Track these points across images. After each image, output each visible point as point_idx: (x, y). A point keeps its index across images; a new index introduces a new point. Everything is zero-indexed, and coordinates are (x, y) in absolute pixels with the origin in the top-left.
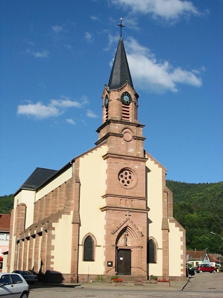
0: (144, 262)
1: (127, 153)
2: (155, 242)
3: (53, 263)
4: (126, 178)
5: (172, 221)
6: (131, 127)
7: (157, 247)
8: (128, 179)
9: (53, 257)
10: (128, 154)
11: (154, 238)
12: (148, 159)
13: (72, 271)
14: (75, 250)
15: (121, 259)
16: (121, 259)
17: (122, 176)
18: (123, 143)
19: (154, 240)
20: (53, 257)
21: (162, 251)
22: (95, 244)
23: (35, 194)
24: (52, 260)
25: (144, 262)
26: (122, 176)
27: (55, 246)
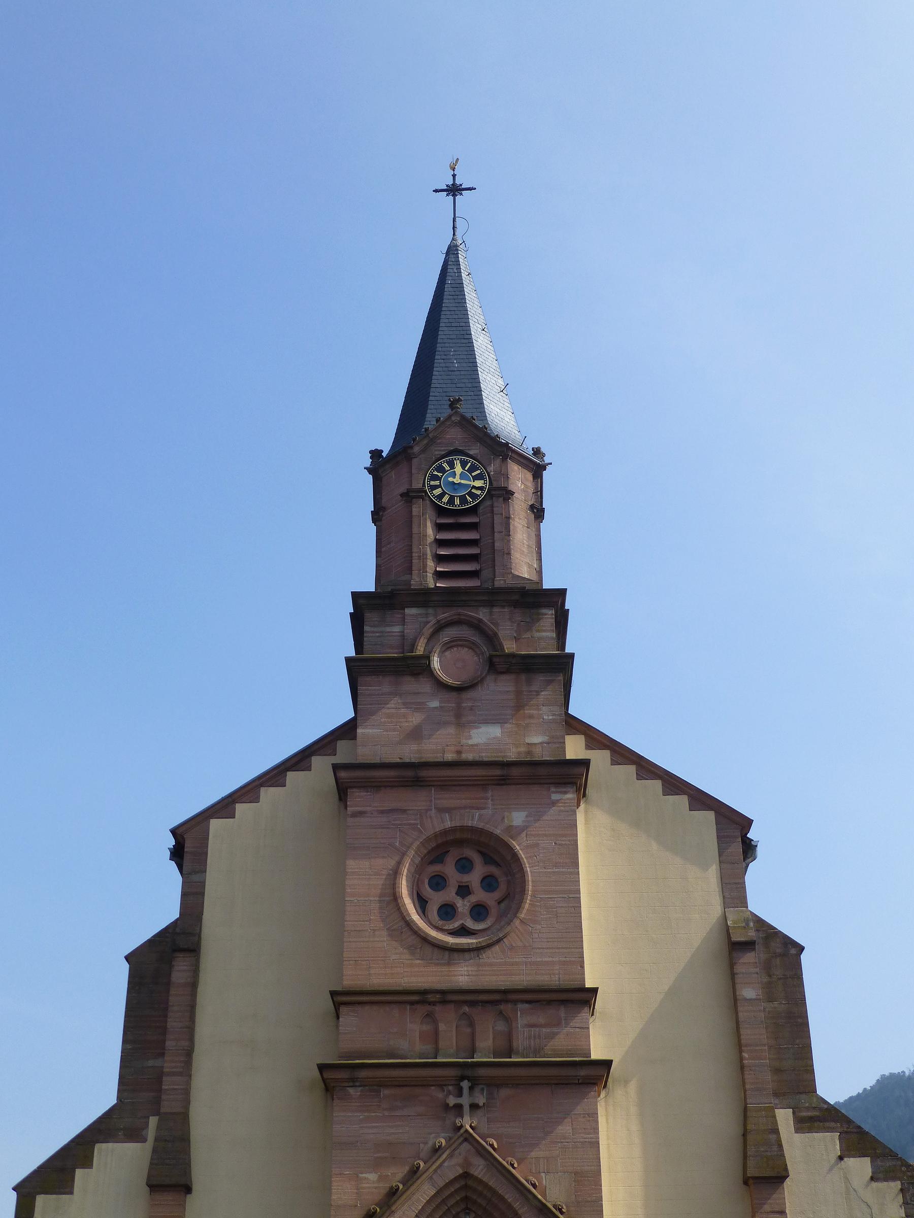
5: (811, 1119)
17: (464, 866)
18: (435, 704)
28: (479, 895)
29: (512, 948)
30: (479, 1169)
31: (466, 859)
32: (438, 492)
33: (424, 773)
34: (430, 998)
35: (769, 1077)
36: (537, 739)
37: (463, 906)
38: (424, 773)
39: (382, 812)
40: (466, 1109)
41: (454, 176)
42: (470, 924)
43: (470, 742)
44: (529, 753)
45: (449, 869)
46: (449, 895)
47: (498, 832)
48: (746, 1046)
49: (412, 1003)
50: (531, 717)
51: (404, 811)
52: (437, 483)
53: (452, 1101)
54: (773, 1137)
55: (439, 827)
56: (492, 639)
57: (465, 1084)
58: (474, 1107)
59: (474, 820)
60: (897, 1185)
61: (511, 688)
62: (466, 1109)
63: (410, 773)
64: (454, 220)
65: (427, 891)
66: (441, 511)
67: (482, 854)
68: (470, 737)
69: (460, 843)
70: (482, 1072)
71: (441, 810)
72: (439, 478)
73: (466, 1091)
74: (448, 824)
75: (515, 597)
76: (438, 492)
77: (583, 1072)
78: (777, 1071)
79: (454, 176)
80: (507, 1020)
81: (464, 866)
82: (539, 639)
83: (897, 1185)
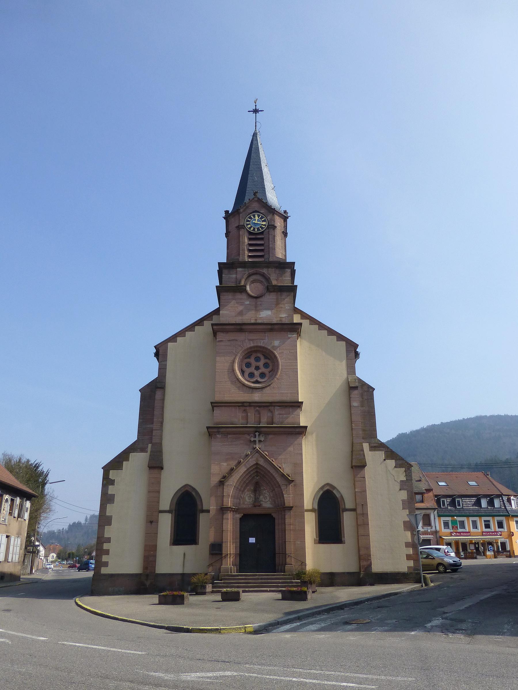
0: (299, 543)
1: (256, 320)
2: (337, 496)
3: (107, 552)
4: (257, 368)
5: (375, 447)
6: (265, 271)
7: (342, 507)
8: (263, 370)
9: (108, 540)
10: (259, 321)
11: (334, 488)
12: (300, 324)
13: (145, 568)
14: (151, 522)
15: (252, 540)
16: (252, 540)
17: (257, 359)
18: (248, 303)
19: (334, 492)
20: (108, 540)
21: (306, 508)
22: (199, 507)
23: (162, 370)
24: (106, 546)
25: (299, 543)
26: (248, 365)
27: (193, 546)
28: (263, 370)
30: (261, 462)
32: (249, 226)
33: (244, 327)
35: (361, 433)
36: (283, 315)
39: (229, 340)
40: (257, 442)
42: (259, 380)
43: (260, 316)
45: (252, 360)
47: (269, 348)
56: (268, 280)
58: (260, 441)
59: (261, 344)
60: (404, 469)
62: (257, 442)
63: (238, 327)
65: (244, 368)
66: (250, 233)
69: (256, 352)
71: (250, 340)
74: (252, 345)
76: (249, 226)
78: (364, 430)
81: (257, 359)
83: (404, 469)
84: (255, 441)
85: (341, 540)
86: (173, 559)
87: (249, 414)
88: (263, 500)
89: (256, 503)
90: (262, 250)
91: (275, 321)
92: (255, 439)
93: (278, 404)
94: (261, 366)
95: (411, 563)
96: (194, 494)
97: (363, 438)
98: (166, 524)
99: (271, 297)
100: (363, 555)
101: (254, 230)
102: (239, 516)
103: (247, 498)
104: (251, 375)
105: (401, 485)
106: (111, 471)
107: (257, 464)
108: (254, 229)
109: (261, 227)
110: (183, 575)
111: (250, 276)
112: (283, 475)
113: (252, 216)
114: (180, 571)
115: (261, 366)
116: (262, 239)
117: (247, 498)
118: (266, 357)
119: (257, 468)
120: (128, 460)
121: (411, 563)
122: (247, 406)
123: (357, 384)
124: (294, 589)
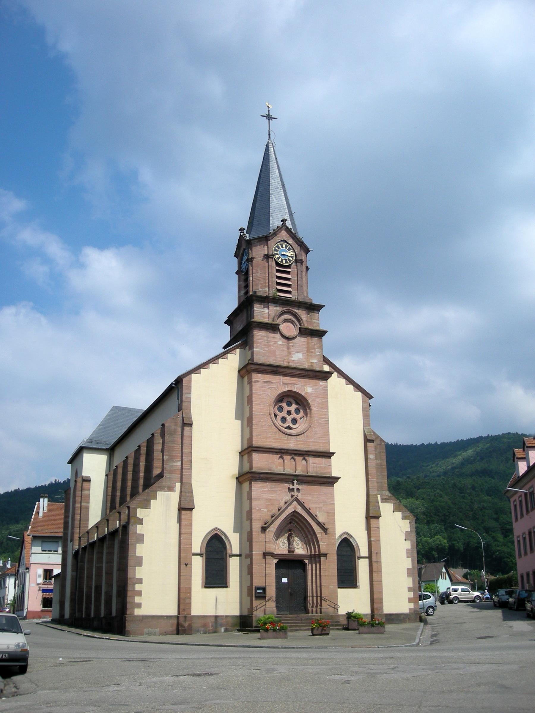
1: (289, 362)
2: (354, 544)
4: (289, 413)
5: (386, 499)
8: (294, 415)
11: (351, 536)
14: (184, 564)
17: (289, 404)
18: (280, 343)
22: (229, 551)
27: (225, 589)
28: (294, 415)
29: (307, 436)
30: (299, 510)
31: (290, 402)
32: (277, 256)
33: (279, 369)
34: (283, 451)
35: (376, 485)
36: (314, 361)
37: (289, 418)
38: (279, 369)
39: (265, 382)
40: (295, 490)
41: (269, 111)
42: (292, 426)
43: (293, 359)
44: (312, 366)
45: (284, 405)
46: (284, 414)
47: (303, 394)
48: (185, 469)
49: (276, 452)
50: (312, 352)
51: (272, 382)
52: (277, 252)
53: (291, 487)
54: (377, 504)
55: (284, 390)
56: (299, 320)
57: (295, 482)
58: (298, 489)
59: (295, 389)
60: (409, 521)
61: (306, 341)
62: (295, 490)
63: (275, 369)
64: (269, 132)
65: (277, 412)
66: (277, 264)
67: (295, 401)
68: (292, 357)
69: (288, 396)
70: (300, 478)
71: (284, 384)
72: (277, 251)
73: (295, 484)
74: (287, 389)
75: (308, 306)
76: (277, 256)
77: (330, 480)
78: (377, 483)
79: (269, 111)
80: (306, 460)
81: (289, 404)
82: (314, 322)
83: (409, 521)
84: (293, 489)
85: (356, 584)
86: (207, 602)
87: (286, 461)
88: (296, 546)
89: (291, 551)
90: (278, 284)
91: (306, 366)
92: (293, 487)
93: (312, 453)
94: (293, 412)
95: (412, 606)
96: (223, 537)
97: (378, 490)
98: (198, 566)
99: (301, 341)
100: (375, 600)
101: (282, 261)
102: (275, 561)
103: (281, 544)
104: (284, 420)
105: (406, 535)
106: (138, 510)
107: (295, 512)
108: (282, 260)
109: (288, 259)
110: (216, 617)
111: (283, 313)
112: (319, 524)
113: (280, 246)
114: (213, 614)
115: (293, 412)
116: (288, 273)
117: (281, 544)
118: (297, 403)
119: (292, 515)
120: (156, 499)
121: (412, 606)
122: (283, 453)
123: (373, 438)
124: (450, 654)
